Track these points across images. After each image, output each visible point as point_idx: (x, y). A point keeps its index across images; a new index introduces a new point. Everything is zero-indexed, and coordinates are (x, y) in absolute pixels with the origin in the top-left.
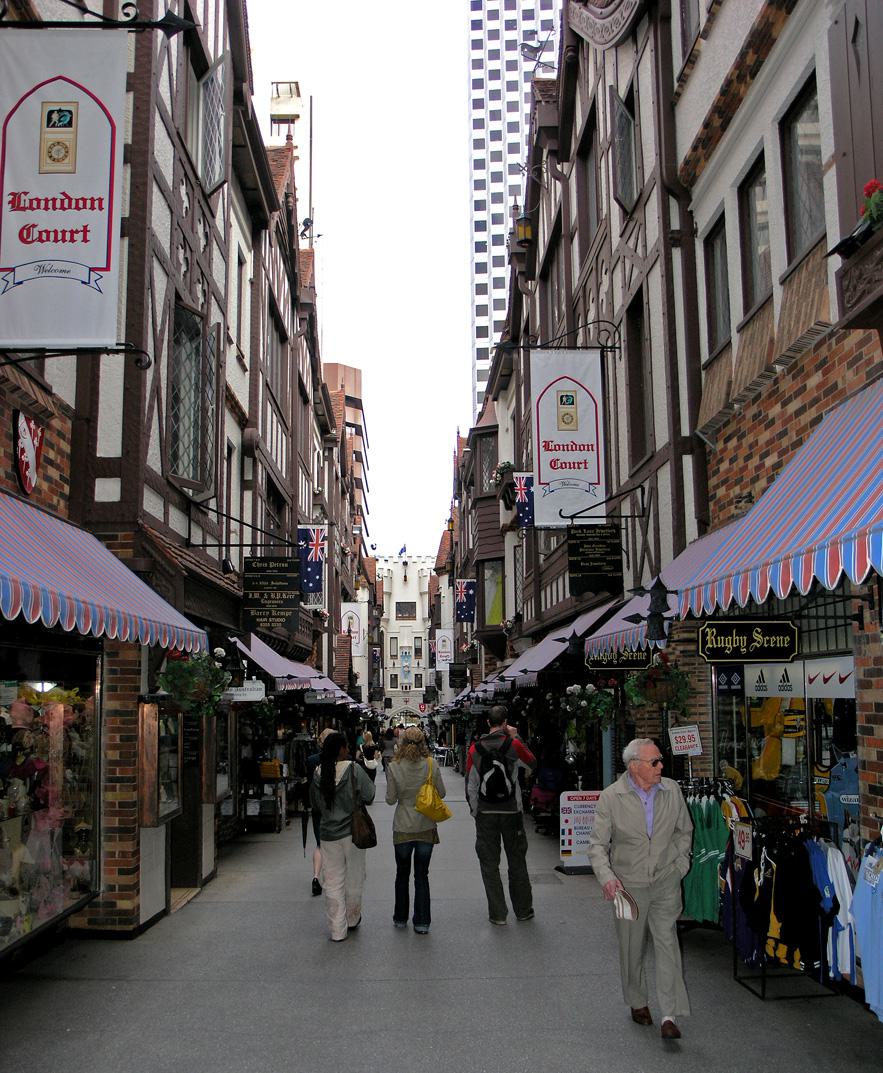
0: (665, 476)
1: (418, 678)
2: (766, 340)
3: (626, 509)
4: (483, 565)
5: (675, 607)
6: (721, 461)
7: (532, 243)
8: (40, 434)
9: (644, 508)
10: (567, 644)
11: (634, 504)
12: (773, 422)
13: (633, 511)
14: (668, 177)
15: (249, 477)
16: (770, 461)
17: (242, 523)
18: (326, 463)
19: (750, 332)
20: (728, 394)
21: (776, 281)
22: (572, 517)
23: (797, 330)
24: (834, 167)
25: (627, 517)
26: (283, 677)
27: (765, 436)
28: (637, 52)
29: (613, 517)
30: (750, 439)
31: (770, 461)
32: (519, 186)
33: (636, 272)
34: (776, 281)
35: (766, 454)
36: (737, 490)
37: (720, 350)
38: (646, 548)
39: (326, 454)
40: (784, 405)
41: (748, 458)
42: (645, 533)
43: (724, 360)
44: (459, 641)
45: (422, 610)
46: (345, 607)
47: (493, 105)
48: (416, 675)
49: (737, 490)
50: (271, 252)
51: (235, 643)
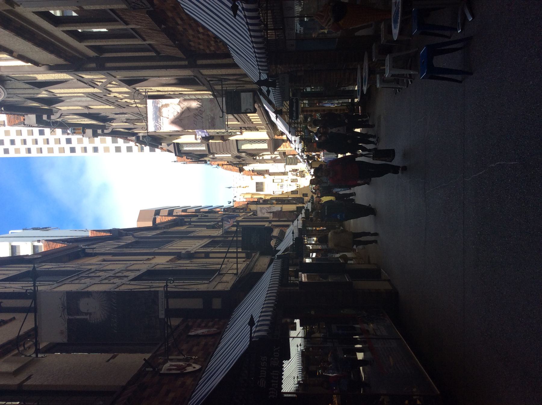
0: (206, 72)
1: (293, 181)
2: (149, 31)
3: (219, 87)
4: (239, 149)
5: (264, 77)
6: (199, 48)
7: (85, 127)
8: (195, 328)
9: (218, 80)
10: (270, 88)
11: (217, 84)
12: (185, 29)
13: (220, 85)
14: (73, 69)
15: (203, 255)
16: (201, 30)
17: (225, 258)
18: (192, 224)
19: (145, 37)
20: (171, 46)
21: (144, 43)
22: (223, 112)
23: (148, 21)
24: (277, 150)
25: (222, 87)
26: (293, 236)
27: (190, 32)
28: (11, 80)
29: (222, 94)
30: (191, 37)
31: (201, 30)
32: (28, 130)
33: (114, 83)
34: (144, 43)
35: (198, 31)
36: (212, 43)
37: (151, 48)
38: (236, 80)
39: (188, 224)
40: (178, 25)
41: (199, 38)
42: (230, 80)
43: (156, 46)
44: (275, 160)
45: (259, 179)
46: (260, 215)
47: (29, 144)
48: (292, 181)
49: (212, 43)
50: (99, 248)
51: (277, 255)
